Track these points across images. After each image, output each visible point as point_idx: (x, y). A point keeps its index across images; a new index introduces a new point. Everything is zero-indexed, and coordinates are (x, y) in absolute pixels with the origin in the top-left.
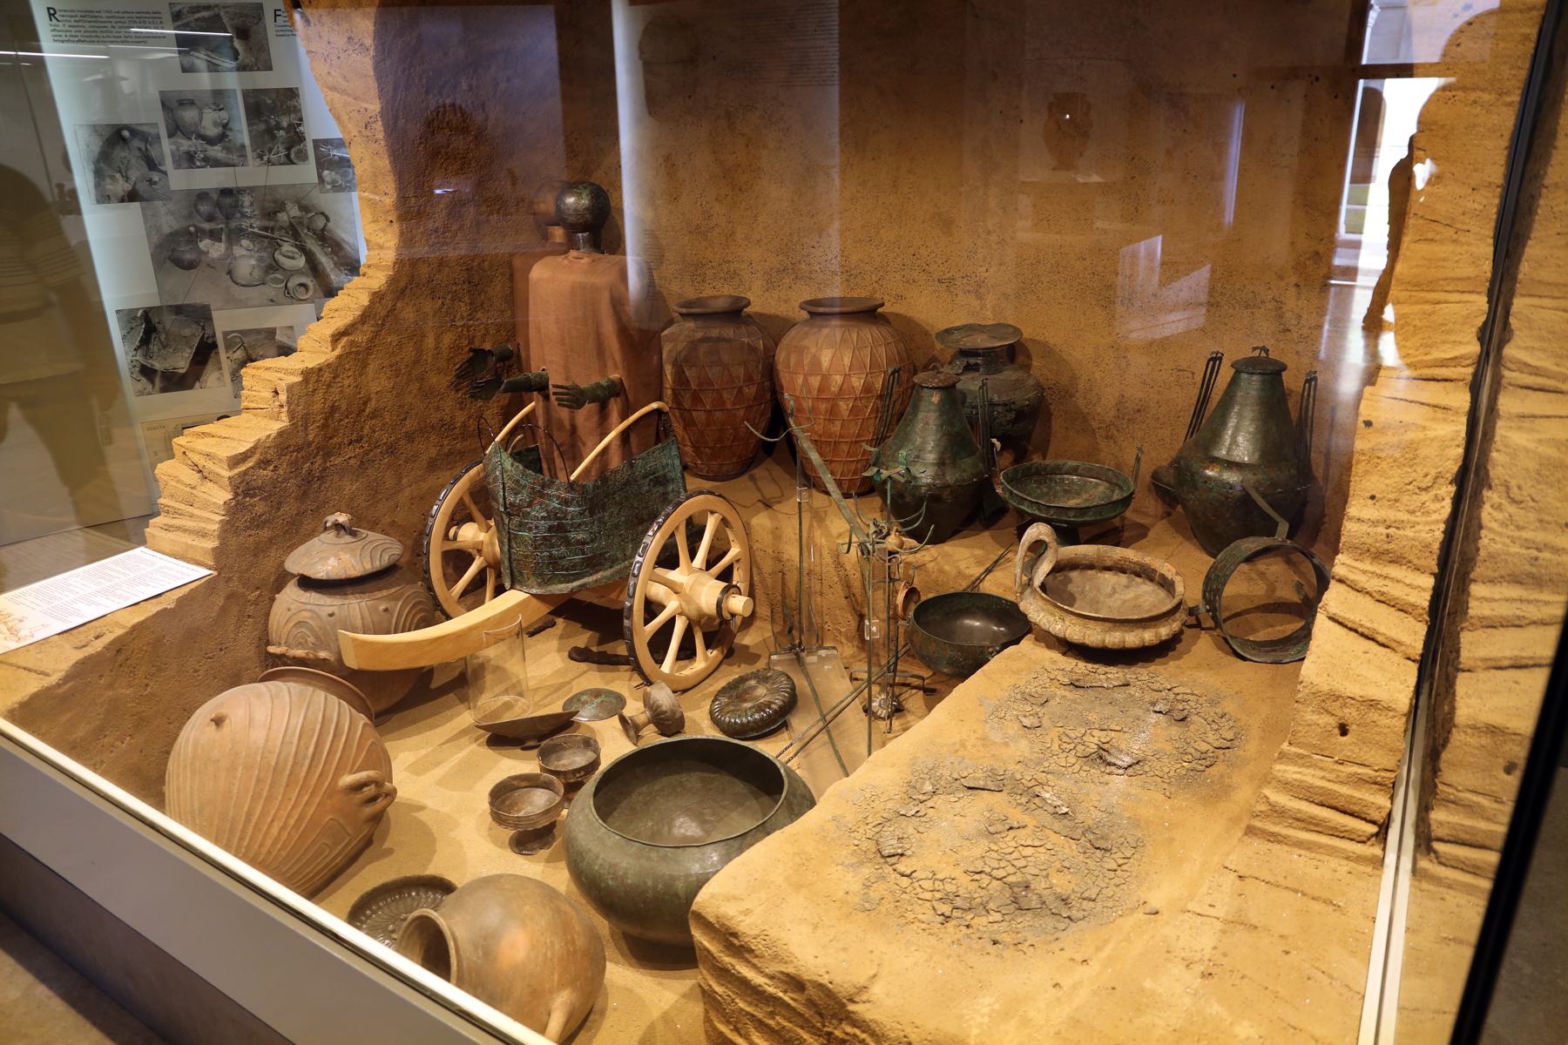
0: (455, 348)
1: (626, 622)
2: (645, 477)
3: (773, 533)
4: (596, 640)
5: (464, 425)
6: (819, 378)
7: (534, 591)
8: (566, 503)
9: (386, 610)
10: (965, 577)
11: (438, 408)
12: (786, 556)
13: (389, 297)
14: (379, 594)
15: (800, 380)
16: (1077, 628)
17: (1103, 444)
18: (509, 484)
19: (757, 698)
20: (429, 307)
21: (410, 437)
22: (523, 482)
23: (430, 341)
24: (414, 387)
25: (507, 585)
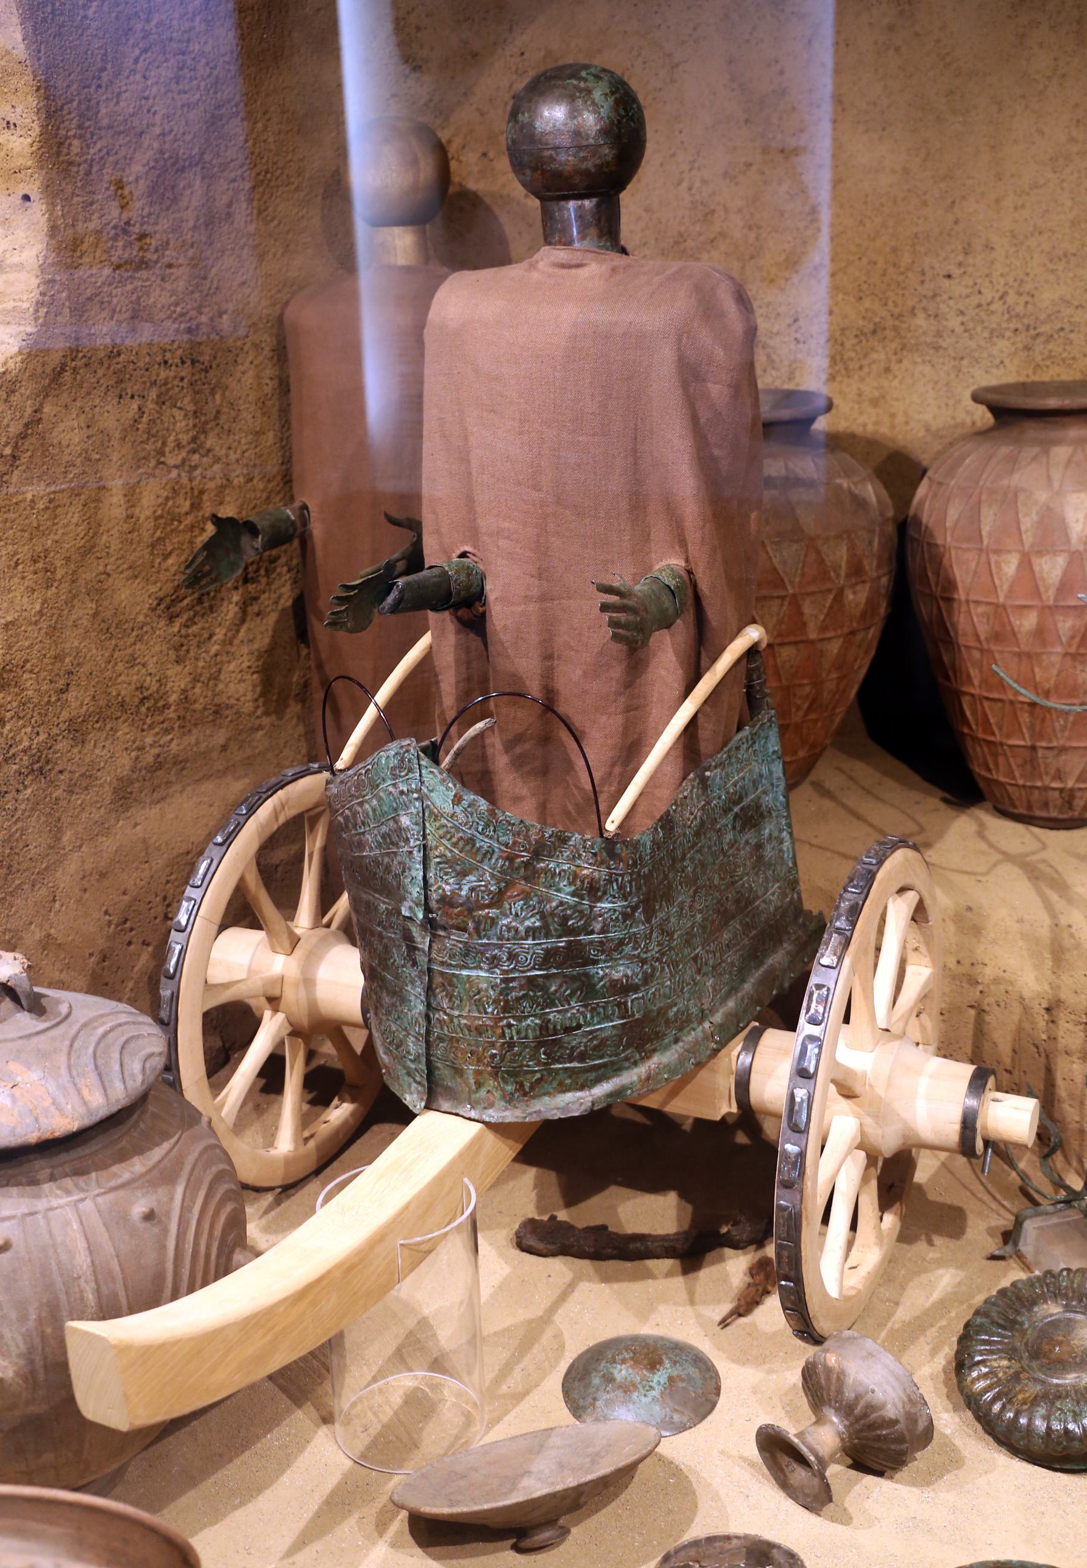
0: (166, 519)
1: (781, 1199)
2: (726, 811)
4: (555, 1194)
5: (186, 699)
6: (1061, 561)
7: (493, 1115)
8: (593, 890)
9: (149, 1216)
11: (132, 661)
12: (988, 973)
13: (27, 389)
14: (125, 1172)
15: (1010, 566)
18: (442, 848)
20: (112, 416)
21: (77, 731)
22: (483, 843)
23: (114, 505)
24: (84, 610)
25: (412, 1099)
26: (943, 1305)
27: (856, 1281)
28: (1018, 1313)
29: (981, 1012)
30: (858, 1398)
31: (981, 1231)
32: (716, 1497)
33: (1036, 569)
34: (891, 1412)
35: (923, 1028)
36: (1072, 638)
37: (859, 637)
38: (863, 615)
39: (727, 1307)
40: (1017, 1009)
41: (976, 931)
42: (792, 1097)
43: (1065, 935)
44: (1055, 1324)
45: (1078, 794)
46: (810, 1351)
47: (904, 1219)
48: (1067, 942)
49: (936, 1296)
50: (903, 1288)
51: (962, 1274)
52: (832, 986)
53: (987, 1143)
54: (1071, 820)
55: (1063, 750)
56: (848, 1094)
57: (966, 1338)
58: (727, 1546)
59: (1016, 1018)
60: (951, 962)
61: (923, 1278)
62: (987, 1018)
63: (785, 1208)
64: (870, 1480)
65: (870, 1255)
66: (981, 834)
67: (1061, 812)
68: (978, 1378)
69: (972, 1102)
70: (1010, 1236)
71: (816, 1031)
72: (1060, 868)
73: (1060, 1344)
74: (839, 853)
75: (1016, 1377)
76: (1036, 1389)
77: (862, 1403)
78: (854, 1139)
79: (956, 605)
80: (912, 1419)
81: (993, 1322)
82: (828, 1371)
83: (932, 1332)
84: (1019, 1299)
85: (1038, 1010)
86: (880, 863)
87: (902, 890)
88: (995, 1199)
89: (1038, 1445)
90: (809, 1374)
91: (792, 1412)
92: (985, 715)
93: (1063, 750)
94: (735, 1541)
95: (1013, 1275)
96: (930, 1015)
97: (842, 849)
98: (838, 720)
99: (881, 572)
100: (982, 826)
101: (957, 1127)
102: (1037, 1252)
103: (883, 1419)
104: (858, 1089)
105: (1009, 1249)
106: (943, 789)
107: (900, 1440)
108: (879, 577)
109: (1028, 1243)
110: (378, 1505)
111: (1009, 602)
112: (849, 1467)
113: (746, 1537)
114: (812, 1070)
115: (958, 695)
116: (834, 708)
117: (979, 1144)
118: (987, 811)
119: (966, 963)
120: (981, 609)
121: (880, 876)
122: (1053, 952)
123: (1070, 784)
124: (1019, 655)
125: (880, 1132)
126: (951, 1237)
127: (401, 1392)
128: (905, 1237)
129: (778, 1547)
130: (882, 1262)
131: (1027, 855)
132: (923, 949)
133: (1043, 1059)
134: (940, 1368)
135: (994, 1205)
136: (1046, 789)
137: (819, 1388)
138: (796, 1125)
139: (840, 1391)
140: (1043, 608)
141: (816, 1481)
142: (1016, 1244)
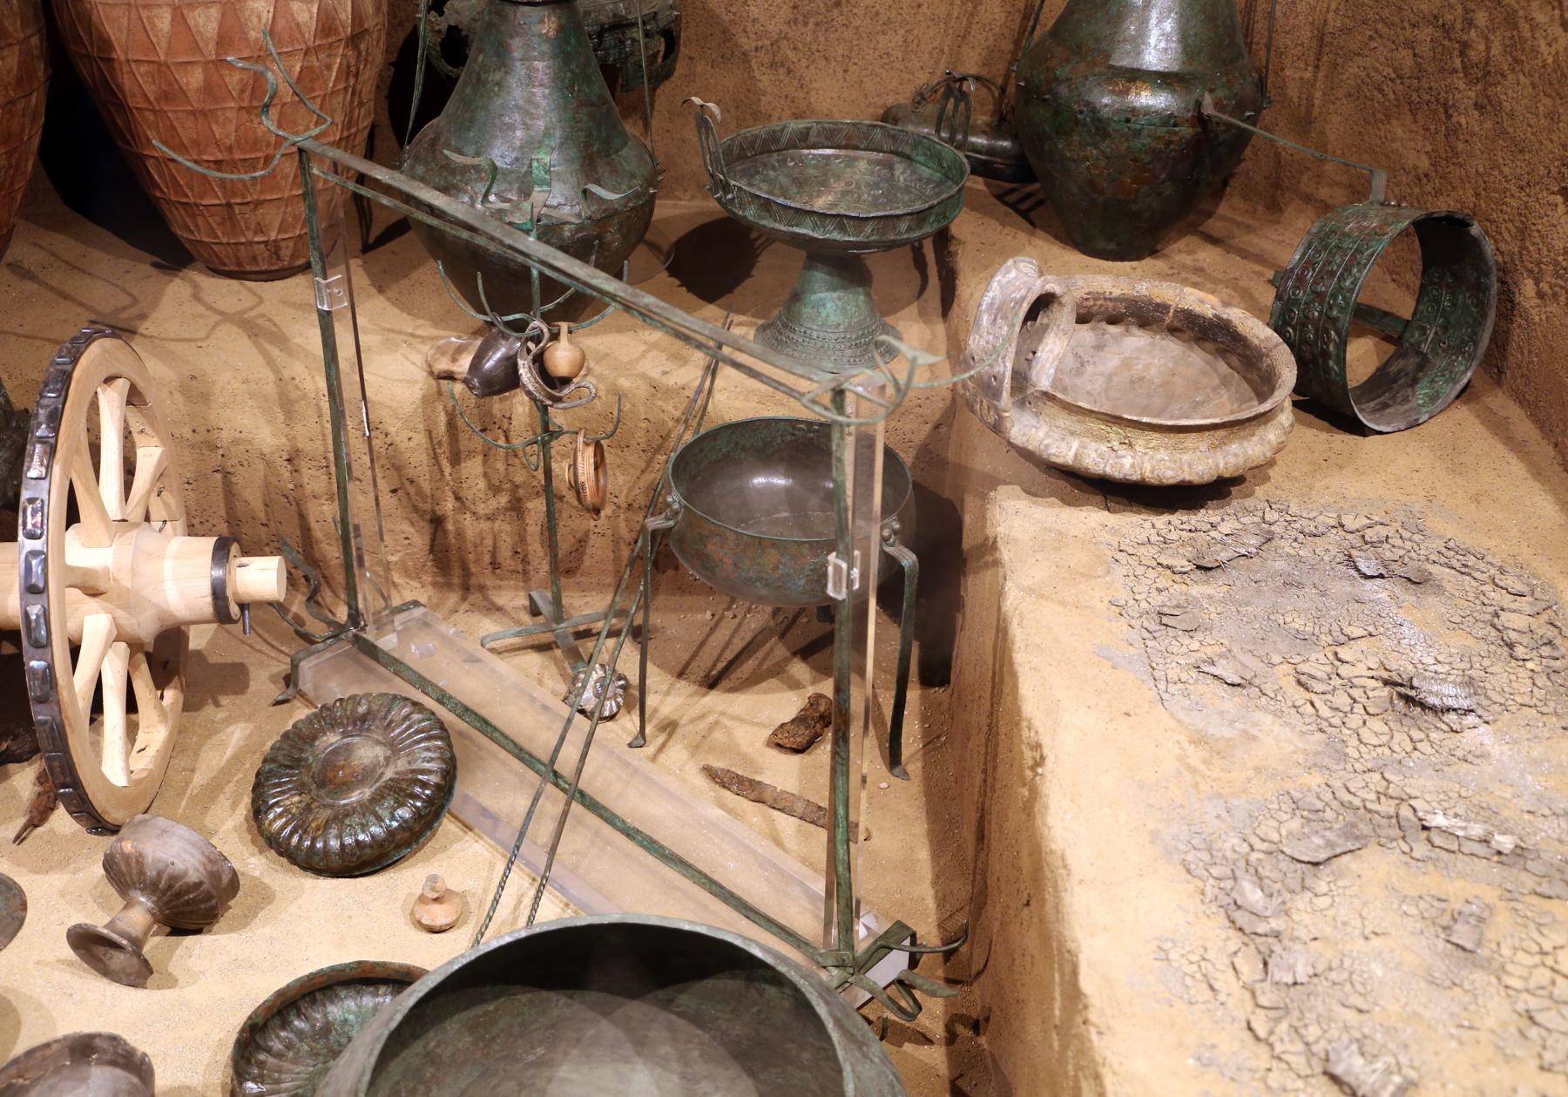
1: (40, 714)
3: (184, 389)
10: (669, 392)
12: (226, 436)
15: (164, 21)
16: (1163, 454)
17: (765, 80)
19: (367, 775)
26: (237, 759)
27: (143, 763)
28: (302, 751)
29: (227, 475)
30: (159, 874)
31: (263, 683)
32: (39, 1006)
33: (191, 23)
34: (193, 877)
35: (166, 505)
36: (243, 91)
37: (20, 106)
38: (19, 81)
39: (20, 822)
40: (261, 466)
41: (205, 397)
42: (26, 615)
43: (290, 388)
44: (336, 752)
45: (283, 244)
46: (105, 843)
47: (186, 690)
48: (294, 395)
49: (229, 753)
50: (197, 754)
51: (251, 726)
52: (45, 498)
53: (243, 606)
54: (283, 269)
55: (258, 204)
56: (94, 593)
57: (259, 789)
58: (48, 1052)
59: (261, 474)
60: (186, 432)
61: (215, 740)
62: (234, 479)
63: (46, 722)
64: (190, 940)
65: (154, 734)
66: (197, 297)
67: (271, 264)
68: (275, 820)
69: (218, 573)
70: (290, 679)
71: (37, 545)
72: (277, 320)
73: (342, 768)
74: (49, 340)
75: (308, 808)
76: (325, 814)
77: (165, 877)
78: (110, 632)
79: (116, 65)
80: (215, 876)
81: (281, 765)
82: (127, 858)
83: (230, 788)
84: (300, 738)
85: (280, 462)
86: (75, 361)
87: (109, 380)
88: (273, 647)
89: (336, 862)
90: (110, 865)
91: (103, 905)
92: (173, 176)
93: (258, 204)
94: (55, 1046)
95: (301, 713)
96: (171, 492)
97: (51, 336)
98: (19, 197)
99: (29, 32)
100: (196, 287)
101: (209, 599)
102: (316, 687)
103: (188, 885)
104: (102, 586)
105: (291, 691)
106: (152, 253)
107: (209, 897)
108: (28, 38)
109: (307, 680)
111: (170, 60)
112: (169, 934)
113: (65, 1038)
114: (41, 585)
115: (141, 159)
116: (12, 184)
117: (234, 610)
118: (200, 271)
119: (202, 430)
120: (143, 69)
121: (76, 375)
122: (282, 407)
123: (273, 236)
124: (193, 113)
125: (134, 621)
126: (235, 693)
128: (190, 705)
129: (98, 1036)
130: (170, 737)
131: (245, 312)
132: (148, 430)
133: (294, 508)
134: (242, 818)
135: (273, 653)
136: (251, 243)
137: (122, 875)
138: (36, 641)
139: (141, 873)
140: (207, 63)
141: (135, 960)
142: (296, 685)
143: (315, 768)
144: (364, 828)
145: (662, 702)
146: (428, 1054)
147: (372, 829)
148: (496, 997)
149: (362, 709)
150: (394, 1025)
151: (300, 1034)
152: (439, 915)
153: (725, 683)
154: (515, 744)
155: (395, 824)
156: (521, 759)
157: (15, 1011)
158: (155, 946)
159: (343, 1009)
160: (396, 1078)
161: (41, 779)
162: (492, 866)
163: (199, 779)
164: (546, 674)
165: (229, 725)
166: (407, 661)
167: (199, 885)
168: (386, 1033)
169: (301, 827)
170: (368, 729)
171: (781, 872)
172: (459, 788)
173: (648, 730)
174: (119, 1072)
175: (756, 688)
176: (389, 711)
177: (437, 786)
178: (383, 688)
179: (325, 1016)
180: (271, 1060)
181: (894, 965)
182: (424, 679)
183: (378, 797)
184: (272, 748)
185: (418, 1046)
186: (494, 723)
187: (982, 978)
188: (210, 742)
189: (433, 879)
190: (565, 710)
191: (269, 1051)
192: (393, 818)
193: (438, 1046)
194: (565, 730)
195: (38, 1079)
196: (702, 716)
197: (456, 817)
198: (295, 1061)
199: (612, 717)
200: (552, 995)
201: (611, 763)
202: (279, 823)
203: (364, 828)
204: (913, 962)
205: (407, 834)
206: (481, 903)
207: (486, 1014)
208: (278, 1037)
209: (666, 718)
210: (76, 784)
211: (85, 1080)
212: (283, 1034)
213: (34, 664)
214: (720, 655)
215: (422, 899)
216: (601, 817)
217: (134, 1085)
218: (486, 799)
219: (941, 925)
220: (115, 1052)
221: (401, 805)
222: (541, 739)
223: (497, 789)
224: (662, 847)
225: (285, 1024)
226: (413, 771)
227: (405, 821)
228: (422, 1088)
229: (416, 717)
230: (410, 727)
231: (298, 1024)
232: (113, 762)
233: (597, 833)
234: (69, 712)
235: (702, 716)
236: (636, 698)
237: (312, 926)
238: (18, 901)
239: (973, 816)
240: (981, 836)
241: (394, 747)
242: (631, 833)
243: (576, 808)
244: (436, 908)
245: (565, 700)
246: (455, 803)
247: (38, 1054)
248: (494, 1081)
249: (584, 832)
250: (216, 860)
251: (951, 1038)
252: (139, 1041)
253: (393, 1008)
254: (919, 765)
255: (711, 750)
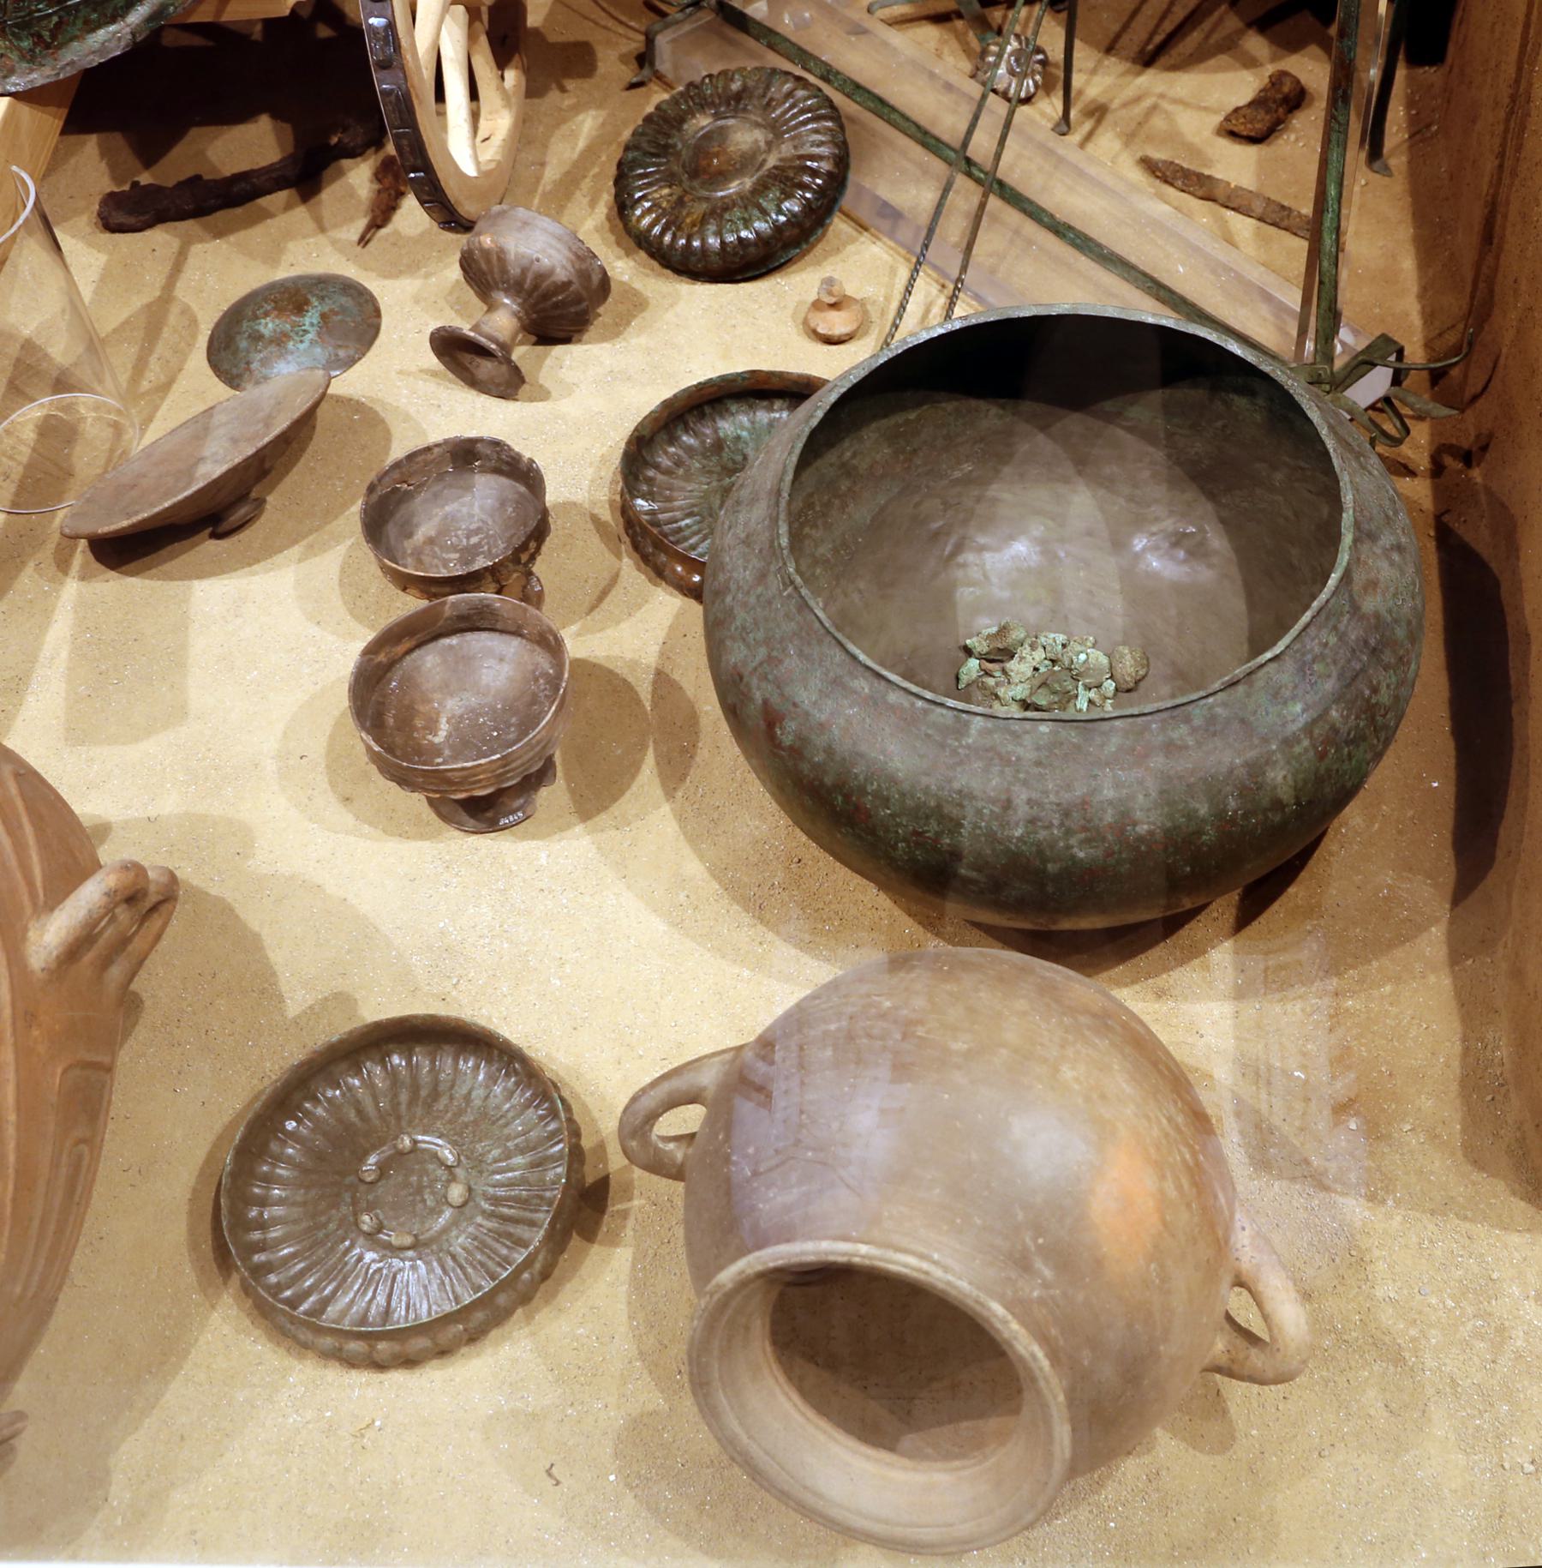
1: (383, 83)
19: (747, 162)
26: (590, 152)
27: (491, 153)
28: (668, 136)
30: (524, 271)
31: (612, 63)
32: (407, 418)
34: (561, 275)
39: (361, 223)
44: (708, 136)
46: (462, 239)
49: (581, 144)
50: (545, 146)
58: (430, 457)
61: (564, 129)
64: (558, 350)
65: (500, 123)
68: (643, 216)
70: (644, 59)
75: (680, 202)
80: (584, 275)
82: (486, 253)
83: (586, 184)
88: (621, 22)
94: (436, 450)
95: (658, 96)
102: (676, 68)
105: (646, 72)
107: (578, 300)
109: (665, 61)
110: (51, 546)
112: (535, 344)
113: (446, 442)
127: (31, 426)
128: (533, 91)
134: (603, 217)
135: (621, 30)
137: (482, 275)
139: (504, 271)
142: (652, 64)
143: (686, 155)
144: (747, 224)
145: (1088, 82)
146: (843, 465)
147: (757, 225)
148: (919, 405)
149: (736, 86)
150: (814, 422)
151: (689, 450)
152: (837, 323)
153: (1164, 60)
154: (918, 127)
155: (782, 219)
156: (925, 145)
157: (383, 421)
158: (521, 354)
159: (735, 424)
160: (809, 490)
161: (378, 176)
162: (893, 271)
163: (551, 174)
164: (946, 50)
165: (577, 114)
166: (779, 30)
167: (566, 285)
168: (807, 431)
169: (673, 224)
170: (745, 110)
171: (1239, 278)
172: (852, 177)
173: (1073, 114)
174: (504, 481)
175: (1202, 66)
176: (768, 88)
177: (829, 173)
178: (750, 65)
179: (716, 431)
180: (660, 477)
181: (1374, 385)
182: (804, 52)
183: (761, 188)
184: (633, 134)
185: (831, 457)
186: (892, 102)
187: (1481, 404)
188: (558, 133)
189: (829, 282)
190: (975, 89)
191: (657, 467)
192: (780, 212)
193: (854, 455)
194: (976, 118)
195: (422, 485)
196: (1137, 99)
197: (848, 216)
198: (688, 477)
199: (1028, 100)
200: (982, 405)
201: (1031, 153)
202: (646, 221)
203: (747, 224)
204: (1397, 380)
205: (796, 231)
206: (883, 313)
207: (907, 422)
208: (666, 453)
209: (1093, 101)
210: (427, 167)
211: (469, 488)
212: (672, 450)
213: (373, 21)
214: (1158, 26)
215: (817, 305)
216: (1024, 211)
217: (521, 495)
218: (885, 192)
219: (1428, 345)
220: (499, 459)
221: (789, 196)
222: (949, 122)
223: (901, 180)
224: (1099, 245)
225: (673, 440)
226: (801, 157)
227: (794, 215)
228: (837, 502)
229: (801, 93)
230: (791, 108)
231: (687, 439)
232: (466, 141)
233: (1017, 232)
234: (414, 80)
235: (1137, 99)
236: (1060, 79)
237: (699, 333)
238: (370, 308)
239: (1477, 213)
240: (1489, 236)
241: (776, 129)
242: (1060, 229)
243: (994, 202)
244: (833, 315)
245: (973, 76)
246: (847, 201)
247: (420, 459)
248: (917, 498)
249: (1005, 228)
250: (584, 258)
251: (1437, 470)
252: (525, 449)
253: (790, 427)
254: (1404, 159)
255: (1149, 139)
